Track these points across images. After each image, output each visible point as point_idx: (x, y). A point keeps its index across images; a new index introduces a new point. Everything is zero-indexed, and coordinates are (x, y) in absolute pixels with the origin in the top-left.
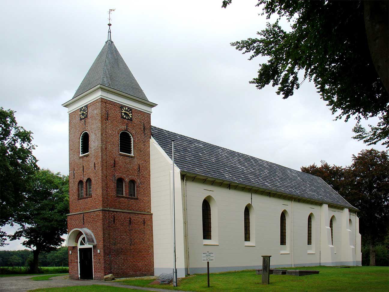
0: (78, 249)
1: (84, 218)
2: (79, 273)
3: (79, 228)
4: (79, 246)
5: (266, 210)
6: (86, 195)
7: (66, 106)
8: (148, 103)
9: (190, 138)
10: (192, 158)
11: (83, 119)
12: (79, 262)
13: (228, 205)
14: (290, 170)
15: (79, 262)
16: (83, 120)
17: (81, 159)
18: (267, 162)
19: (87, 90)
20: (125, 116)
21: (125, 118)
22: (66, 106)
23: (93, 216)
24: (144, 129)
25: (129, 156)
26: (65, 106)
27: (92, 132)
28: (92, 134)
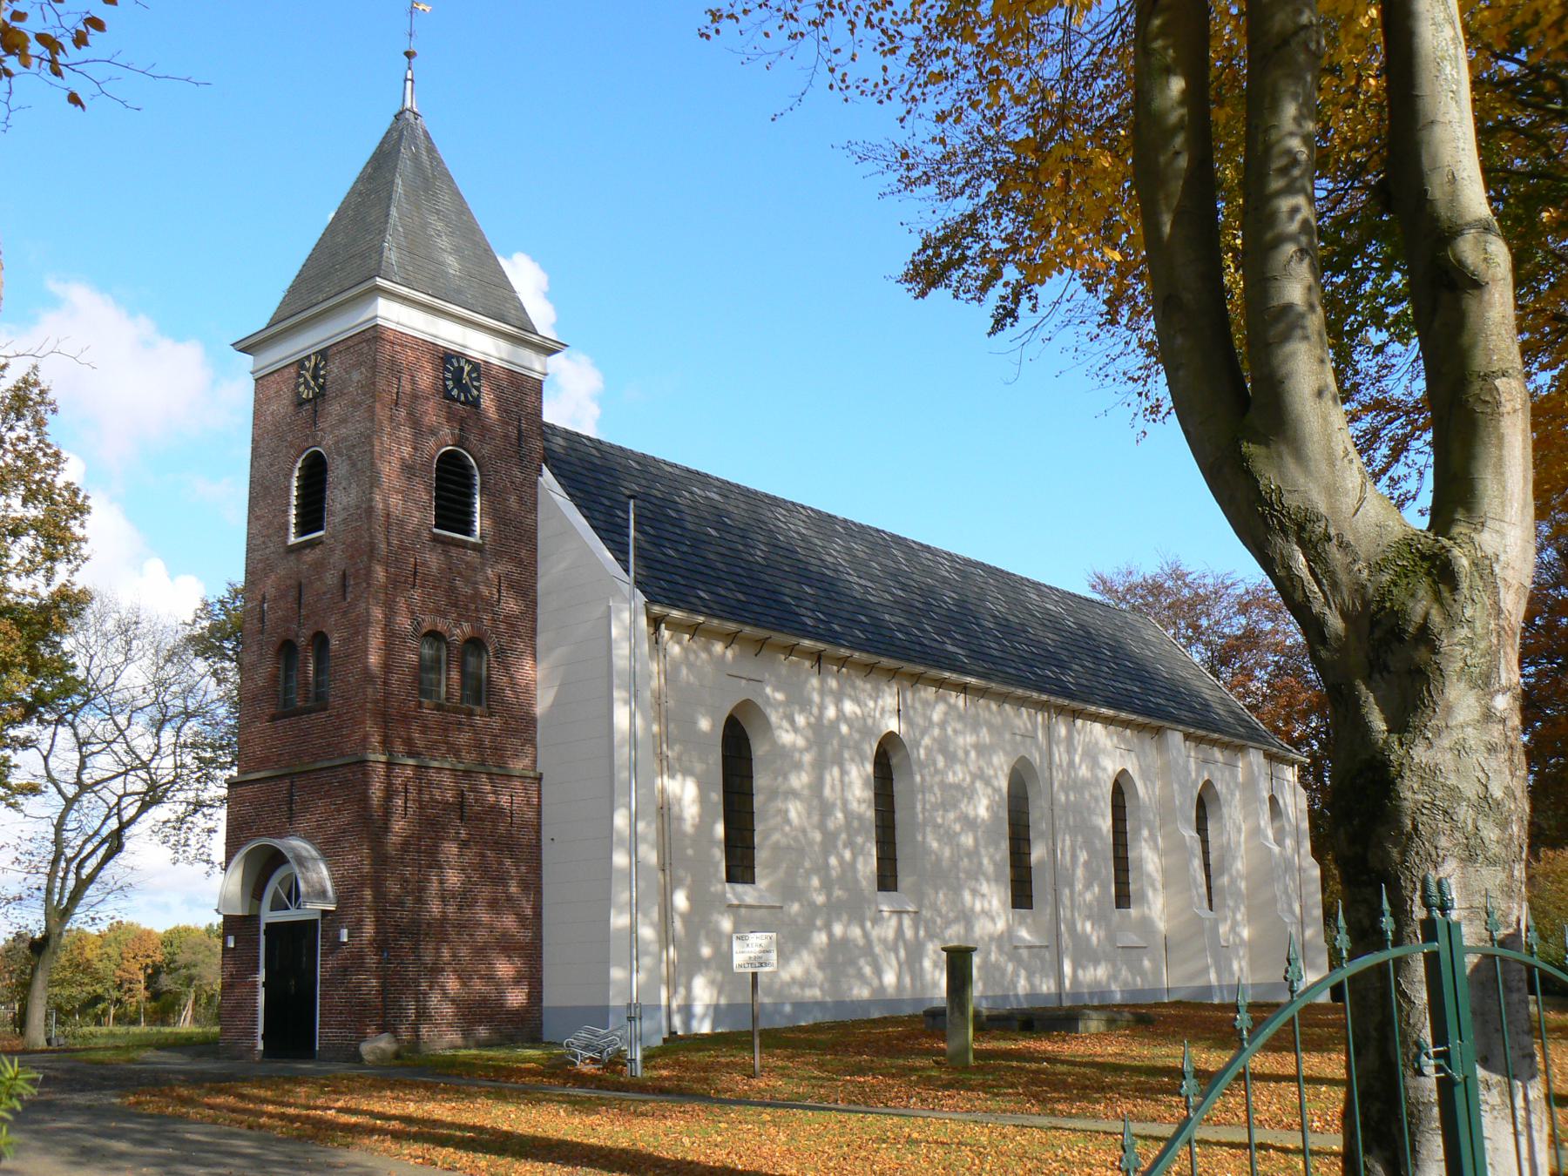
0: (263, 927)
1: (292, 795)
2: (260, 1030)
3: (270, 836)
4: (268, 916)
5: (967, 746)
6: (306, 699)
7: (248, 346)
8: (535, 338)
9: (676, 466)
10: (685, 549)
11: (309, 400)
12: (259, 1038)
13: (826, 722)
14: (1037, 586)
15: (264, 1037)
16: (308, 407)
17: (293, 557)
18: (952, 558)
19: (347, 285)
20: (455, 392)
21: (458, 400)
22: (248, 346)
23: (327, 787)
24: (519, 439)
25: (464, 545)
26: (243, 350)
27: (340, 454)
28: (338, 460)
